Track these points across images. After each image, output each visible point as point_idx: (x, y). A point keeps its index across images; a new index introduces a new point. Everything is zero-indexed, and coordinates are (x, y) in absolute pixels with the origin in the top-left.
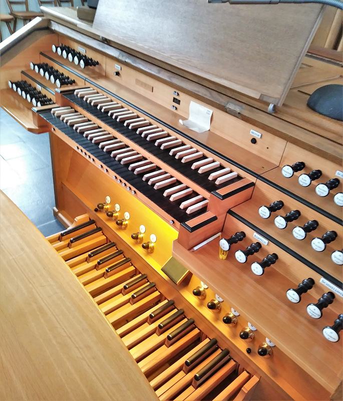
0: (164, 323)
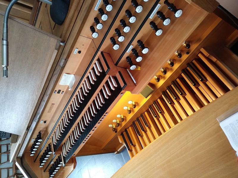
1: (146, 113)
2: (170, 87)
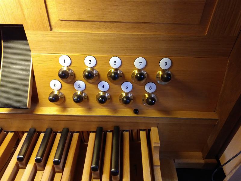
0: (40, 154)
1: (10, 135)
2: (53, 134)
